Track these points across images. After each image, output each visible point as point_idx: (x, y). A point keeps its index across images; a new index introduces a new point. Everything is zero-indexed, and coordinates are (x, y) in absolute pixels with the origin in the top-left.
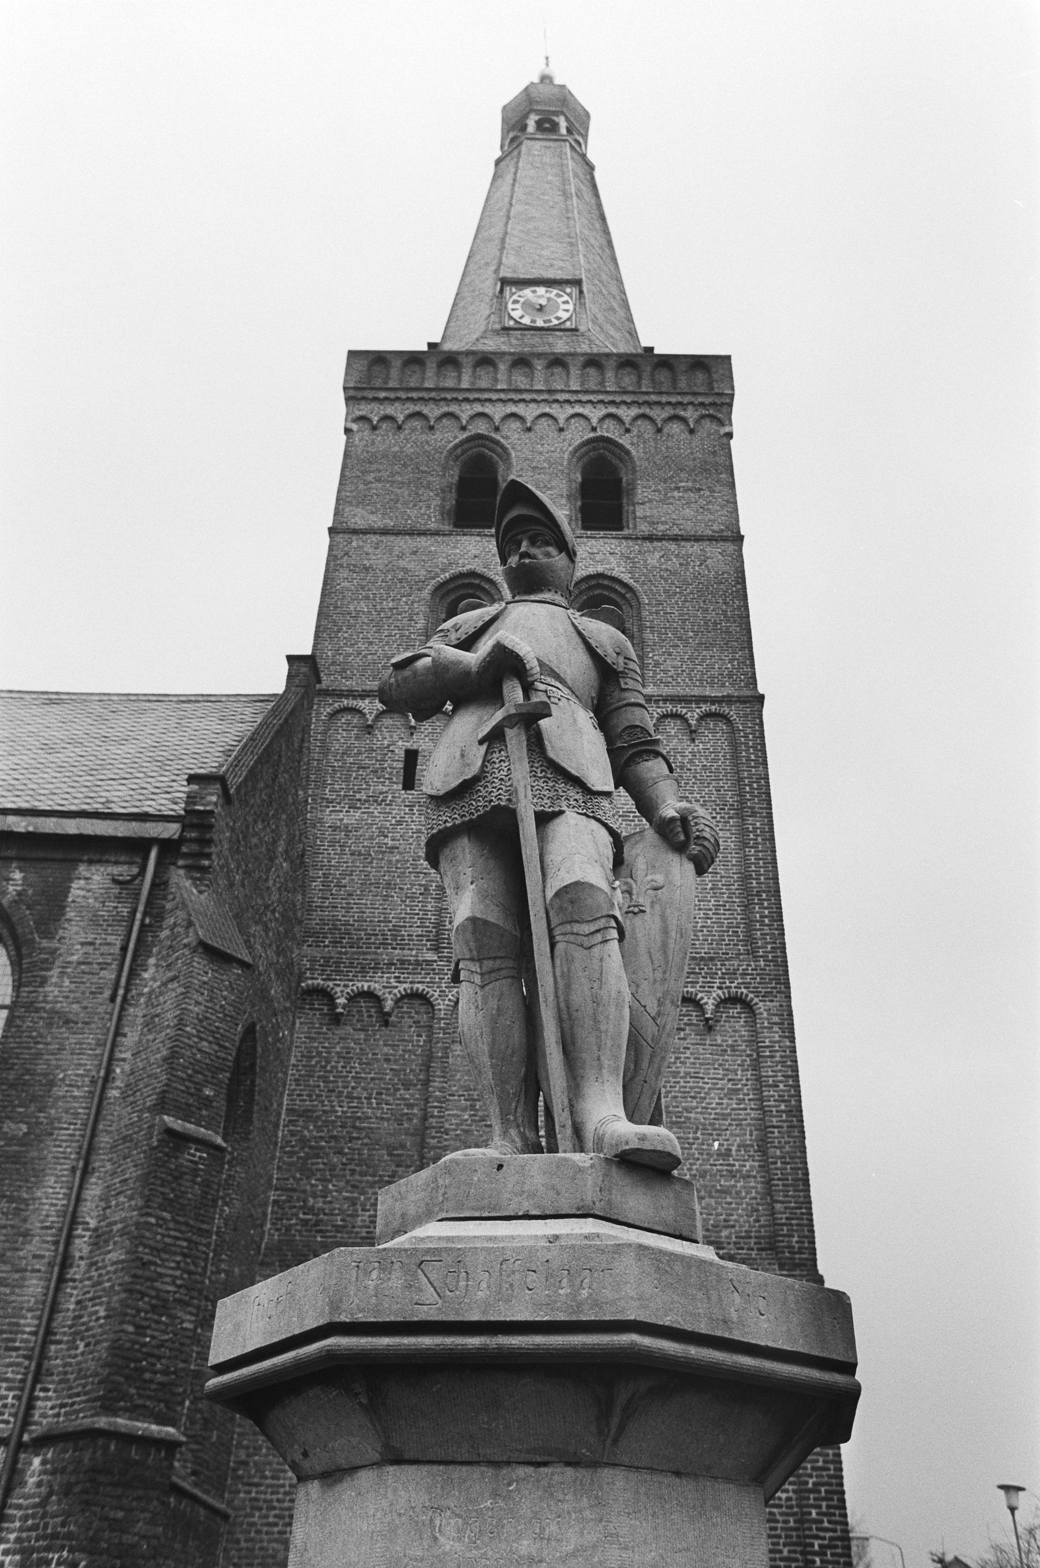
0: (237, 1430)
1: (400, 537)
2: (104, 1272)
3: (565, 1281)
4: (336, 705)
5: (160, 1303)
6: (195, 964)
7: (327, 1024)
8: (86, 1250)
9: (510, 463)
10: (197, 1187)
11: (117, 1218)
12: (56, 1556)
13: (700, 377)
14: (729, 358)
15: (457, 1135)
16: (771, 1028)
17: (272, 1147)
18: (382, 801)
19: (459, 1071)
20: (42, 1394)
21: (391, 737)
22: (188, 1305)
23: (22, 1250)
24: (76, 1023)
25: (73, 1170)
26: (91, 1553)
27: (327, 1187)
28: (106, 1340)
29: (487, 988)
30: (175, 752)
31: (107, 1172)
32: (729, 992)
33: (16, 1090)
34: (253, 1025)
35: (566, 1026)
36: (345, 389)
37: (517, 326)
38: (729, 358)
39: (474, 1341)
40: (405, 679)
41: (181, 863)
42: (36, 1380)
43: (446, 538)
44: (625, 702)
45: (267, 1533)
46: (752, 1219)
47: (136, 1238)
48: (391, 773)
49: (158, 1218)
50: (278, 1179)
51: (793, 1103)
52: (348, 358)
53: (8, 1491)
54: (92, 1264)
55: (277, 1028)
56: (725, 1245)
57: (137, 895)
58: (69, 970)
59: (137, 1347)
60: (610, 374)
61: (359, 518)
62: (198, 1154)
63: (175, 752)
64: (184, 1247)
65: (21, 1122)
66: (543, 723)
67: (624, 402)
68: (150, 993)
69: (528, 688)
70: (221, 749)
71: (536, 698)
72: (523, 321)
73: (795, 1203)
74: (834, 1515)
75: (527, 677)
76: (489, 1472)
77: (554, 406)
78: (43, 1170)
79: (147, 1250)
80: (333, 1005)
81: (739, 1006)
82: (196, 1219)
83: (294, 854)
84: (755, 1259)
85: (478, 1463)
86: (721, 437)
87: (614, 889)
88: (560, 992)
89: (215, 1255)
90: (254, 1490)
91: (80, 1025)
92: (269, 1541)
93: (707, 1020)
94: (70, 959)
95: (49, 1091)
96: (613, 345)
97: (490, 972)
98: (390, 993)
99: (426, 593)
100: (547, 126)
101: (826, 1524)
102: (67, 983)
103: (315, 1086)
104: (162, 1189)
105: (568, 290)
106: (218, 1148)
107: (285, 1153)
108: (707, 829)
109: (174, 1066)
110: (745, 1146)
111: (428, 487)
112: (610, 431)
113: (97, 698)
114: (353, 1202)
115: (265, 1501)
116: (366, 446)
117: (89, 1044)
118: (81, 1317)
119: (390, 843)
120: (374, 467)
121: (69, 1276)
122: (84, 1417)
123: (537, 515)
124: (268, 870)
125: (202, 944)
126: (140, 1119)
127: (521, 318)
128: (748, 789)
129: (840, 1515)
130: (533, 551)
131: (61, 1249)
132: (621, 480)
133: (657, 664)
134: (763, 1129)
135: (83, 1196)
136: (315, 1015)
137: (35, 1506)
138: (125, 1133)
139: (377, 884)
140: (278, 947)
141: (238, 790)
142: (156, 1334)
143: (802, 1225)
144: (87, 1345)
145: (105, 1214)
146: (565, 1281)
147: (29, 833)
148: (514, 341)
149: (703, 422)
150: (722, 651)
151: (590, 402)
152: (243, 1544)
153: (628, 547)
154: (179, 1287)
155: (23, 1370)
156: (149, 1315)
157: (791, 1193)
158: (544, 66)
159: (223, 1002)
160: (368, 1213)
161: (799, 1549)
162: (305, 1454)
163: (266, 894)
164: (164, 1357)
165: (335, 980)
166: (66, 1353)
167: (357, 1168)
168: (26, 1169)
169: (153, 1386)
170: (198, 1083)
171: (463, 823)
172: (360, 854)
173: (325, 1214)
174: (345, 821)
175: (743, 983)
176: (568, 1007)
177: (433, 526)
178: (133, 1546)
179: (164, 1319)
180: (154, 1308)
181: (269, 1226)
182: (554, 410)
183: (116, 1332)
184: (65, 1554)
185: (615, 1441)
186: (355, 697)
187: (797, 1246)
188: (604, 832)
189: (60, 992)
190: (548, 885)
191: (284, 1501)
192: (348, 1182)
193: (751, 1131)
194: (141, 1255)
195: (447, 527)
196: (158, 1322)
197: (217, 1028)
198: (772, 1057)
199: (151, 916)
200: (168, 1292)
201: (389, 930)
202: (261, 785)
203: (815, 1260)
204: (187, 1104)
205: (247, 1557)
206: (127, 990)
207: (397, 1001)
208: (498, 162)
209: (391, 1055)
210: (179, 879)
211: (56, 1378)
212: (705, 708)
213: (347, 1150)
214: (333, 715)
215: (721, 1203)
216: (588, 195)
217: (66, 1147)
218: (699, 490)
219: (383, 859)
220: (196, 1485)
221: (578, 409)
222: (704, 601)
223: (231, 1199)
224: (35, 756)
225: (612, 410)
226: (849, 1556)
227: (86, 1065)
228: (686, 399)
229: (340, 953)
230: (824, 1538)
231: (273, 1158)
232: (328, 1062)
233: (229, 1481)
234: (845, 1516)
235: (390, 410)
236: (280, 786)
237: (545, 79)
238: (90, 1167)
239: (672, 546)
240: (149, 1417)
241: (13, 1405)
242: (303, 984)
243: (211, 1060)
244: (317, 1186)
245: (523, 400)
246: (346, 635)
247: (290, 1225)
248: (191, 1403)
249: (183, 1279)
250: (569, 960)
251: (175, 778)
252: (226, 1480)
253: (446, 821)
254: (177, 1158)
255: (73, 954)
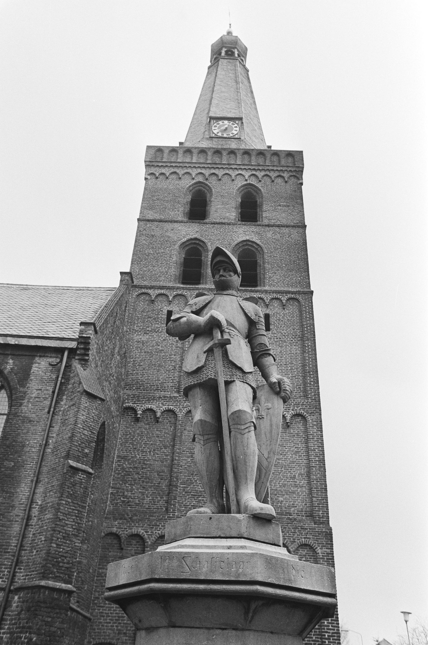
0: (95, 584)
1: (167, 223)
2: (44, 522)
3: (234, 566)
4: (139, 291)
5: (66, 535)
6: (82, 399)
7: (134, 422)
8: (37, 513)
9: (212, 194)
10: (82, 489)
11: (50, 501)
12: (24, 636)
13: (290, 160)
14: (302, 152)
15: (185, 468)
16: (313, 427)
17: (111, 471)
18: (158, 331)
19: (186, 442)
20: (18, 571)
21: (161, 305)
22: (77, 536)
23: (11, 513)
24: (34, 422)
25: (32, 481)
26: (38, 635)
27: (132, 487)
28: (44, 550)
29: (206, 446)
30: (74, 311)
31: (45, 482)
32: (296, 412)
33: (10, 449)
34: (104, 422)
35: (235, 462)
36: (145, 161)
37: (216, 137)
38: (302, 152)
39: (202, 587)
40: (176, 326)
41: (77, 357)
42: (16, 565)
43: (185, 224)
44: (258, 334)
45: (106, 626)
46: (303, 504)
47: (57, 509)
48: (161, 320)
49: (66, 501)
50: (113, 484)
51: (321, 457)
52: (147, 149)
53: (5, 609)
54: (39, 519)
55: (113, 423)
56: (293, 514)
57: (59, 370)
58: (31, 400)
59: (57, 553)
60: (253, 158)
61: (150, 215)
62: (82, 476)
63: (74, 311)
64: (76, 513)
65: (11, 461)
66: (228, 346)
67: (259, 169)
68: (64, 410)
69: (222, 332)
70: (93, 310)
71: (226, 336)
72: (218, 134)
73: (321, 498)
74: (334, 623)
75: (222, 328)
76: (206, 631)
77: (230, 170)
78: (20, 481)
79: (61, 514)
80: (136, 414)
81: (300, 417)
82: (81, 502)
83: (122, 352)
84: (304, 520)
85: (202, 628)
86: (298, 184)
87: (253, 411)
88: (232, 450)
89: (87, 514)
90: (101, 609)
91: (35, 422)
92: (107, 629)
93: (287, 423)
94: (32, 396)
95: (23, 449)
96: (255, 145)
97: (207, 440)
98: (159, 409)
99: (177, 247)
100: (230, 54)
101: (330, 627)
102: (30, 405)
103: (128, 447)
104: (68, 490)
105: (237, 122)
106: (90, 474)
107: (116, 473)
108: (288, 387)
109: (73, 440)
110: (301, 474)
111: (178, 203)
112: (253, 181)
113: (43, 288)
114: (143, 494)
115: (106, 613)
116: (153, 185)
117: (39, 430)
118: (34, 540)
119: (160, 348)
120: (157, 194)
121: (30, 524)
122: (35, 580)
123: (227, 260)
124: (112, 359)
125: (85, 391)
126: (59, 461)
127: (218, 133)
128: (306, 329)
129: (336, 624)
130: (225, 274)
131: (27, 513)
132: (257, 201)
133: (270, 277)
134: (309, 467)
135: (36, 492)
136: (129, 417)
137: (16, 615)
138: (53, 467)
139: (155, 365)
140: (115, 390)
141: (100, 328)
142: (65, 548)
143: (324, 507)
144: (37, 551)
145: (44, 499)
146: (234, 566)
147: (16, 344)
148: (214, 143)
149: (291, 178)
150: (296, 272)
151: (245, 169)
152: (97, 631)
153: (259, 229)
154: (74, 529)
155: (11, 561)
156: (62, 540)
157: (319, 494)
158: (229, 28)
159: (93, 415)
160: (149, 499)
161: (319, 637)
162: (140, 621)
163: (110, 369)
164: (67, 557)
165: (137, 403)
166: (28, 554)
167: (145, 480)
168: (13, 480)
169: (63, 569)
170: (83, 447)
171: (198, 383)
172: (148, 353)
173: (131, 498)
174: (142, 339)
175: (302, 408)
176: (235, 456)
177: (180, 219)
178: (54, 632)
179: (68, 542)
180: (64, 537)
181: (109, 502)
182: (230, 172)
183: (49, 547)
184: (28, 634)
185: (250, 622)
186: (147, 288)
187: (321, 515)
188: (250, 388)
189: (28, 409)
190: (229, 410)
191: (113, 614)
192: (141, 485)
193: (304, 468)
194: (59, 516)
195: (186, 220)
196: (65, 543)
197: (91, 425)
198: (313, 438)
199: (65, 379)
200: (70, 531)
201: (160, 384)
202: (109, 325)
203: (329, 521)
204: (78, 455)
205: (98, 636)
206: (55, 409)
207: (162, 413)
208: (209, 68)
209: (160, 435)
210: (76, 365)
211: (24, 564)
212: (289, 296)
213: (141, 473)
214: (138, 296)
215: (291, 497)
216: (246, 82)
217: (29, 472)
218: (289, 206)
219: (157, 355)
220: (78, 606)
221: (240, 172)
222: (290, 252)
223: (94, 492)
224: (18, 312)
225: (254, 172)
226: (340, 640)
227: (37, 439)
228: (284, 169)
229: (140, 393)
230: (330, 633)
231: (111, 475)
232: (134, 437)
233: (91, 605)
234: (338, 624)
235: (163, 171)
236: (117, 326)
237: (229, 33)
238: (39, 480)
239: (277, 229)
240: (61, 581)
241: (7, 575)
242: (124, 405)
243: (88, 438)
244: (128, 487)
245: (218, 168)
246: (144, 263)
247: (118, 503)
248: (77, 574)
249: (76, 526)
250: (236, 438)
251: (75, 322)
252: (90, 605)
253: (191, 382)
254: (74, 477)
255: (33, 394)
